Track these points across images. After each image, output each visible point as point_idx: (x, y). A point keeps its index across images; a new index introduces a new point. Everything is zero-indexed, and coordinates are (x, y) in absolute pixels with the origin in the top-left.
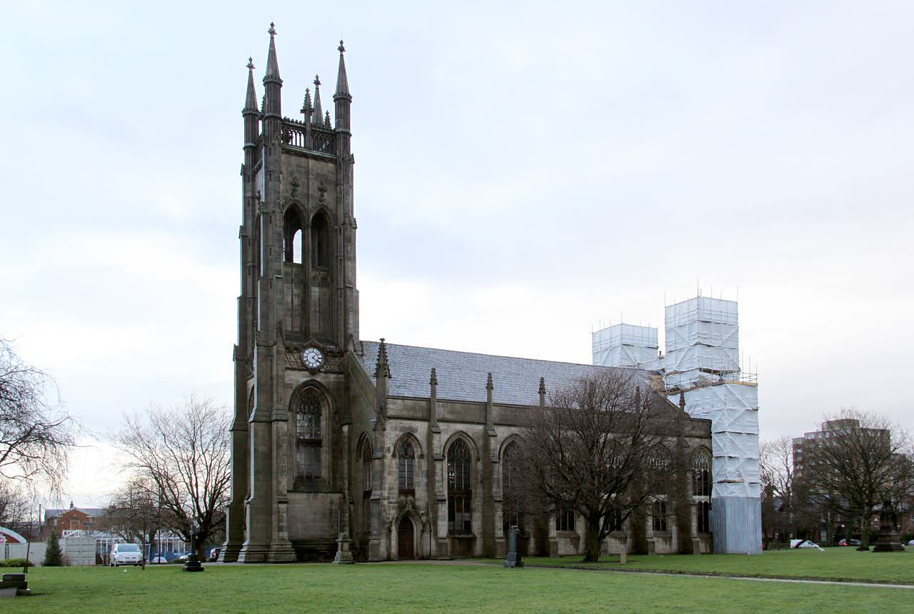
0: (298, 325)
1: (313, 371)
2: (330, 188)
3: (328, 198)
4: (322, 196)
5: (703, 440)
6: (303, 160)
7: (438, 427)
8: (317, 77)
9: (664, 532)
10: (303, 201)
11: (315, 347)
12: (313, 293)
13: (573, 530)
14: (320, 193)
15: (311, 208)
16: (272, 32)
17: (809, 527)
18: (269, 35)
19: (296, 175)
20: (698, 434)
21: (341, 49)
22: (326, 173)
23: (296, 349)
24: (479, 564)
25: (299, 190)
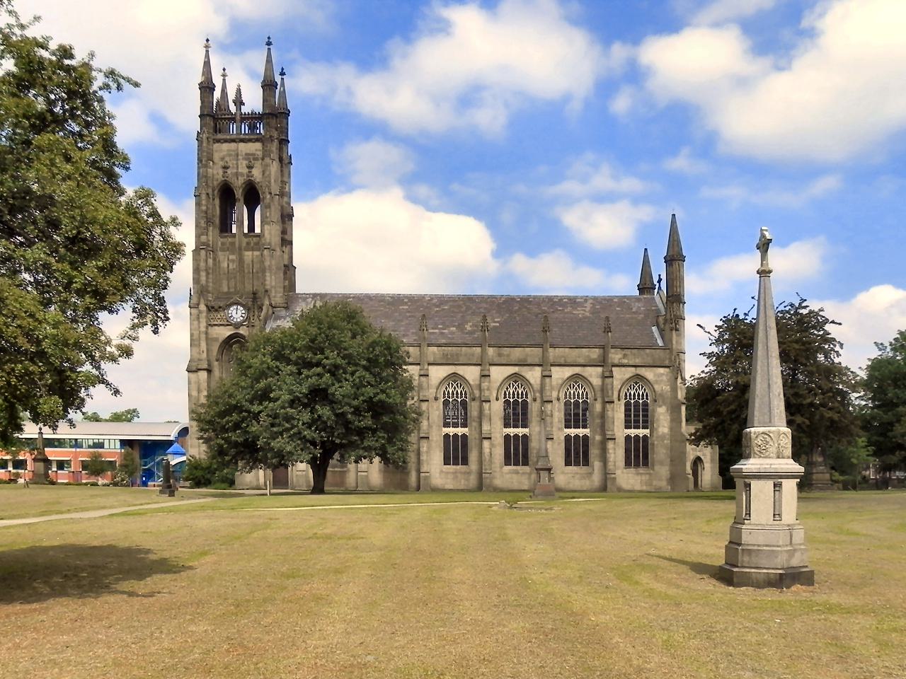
1: (237, 326)
4: (250, 172)
5: (638, 369)
6: (233, 145)
8: (283, 69)
11: (237, 304)
12: (246, 258)
13: (467, 464)
14: (247, 170)
17: (512, 483)
19: (227, 159)
20: (631, 363)
22: (254, 152)
23: (220, 307)
24: (782, 466)
25: (229, 171)
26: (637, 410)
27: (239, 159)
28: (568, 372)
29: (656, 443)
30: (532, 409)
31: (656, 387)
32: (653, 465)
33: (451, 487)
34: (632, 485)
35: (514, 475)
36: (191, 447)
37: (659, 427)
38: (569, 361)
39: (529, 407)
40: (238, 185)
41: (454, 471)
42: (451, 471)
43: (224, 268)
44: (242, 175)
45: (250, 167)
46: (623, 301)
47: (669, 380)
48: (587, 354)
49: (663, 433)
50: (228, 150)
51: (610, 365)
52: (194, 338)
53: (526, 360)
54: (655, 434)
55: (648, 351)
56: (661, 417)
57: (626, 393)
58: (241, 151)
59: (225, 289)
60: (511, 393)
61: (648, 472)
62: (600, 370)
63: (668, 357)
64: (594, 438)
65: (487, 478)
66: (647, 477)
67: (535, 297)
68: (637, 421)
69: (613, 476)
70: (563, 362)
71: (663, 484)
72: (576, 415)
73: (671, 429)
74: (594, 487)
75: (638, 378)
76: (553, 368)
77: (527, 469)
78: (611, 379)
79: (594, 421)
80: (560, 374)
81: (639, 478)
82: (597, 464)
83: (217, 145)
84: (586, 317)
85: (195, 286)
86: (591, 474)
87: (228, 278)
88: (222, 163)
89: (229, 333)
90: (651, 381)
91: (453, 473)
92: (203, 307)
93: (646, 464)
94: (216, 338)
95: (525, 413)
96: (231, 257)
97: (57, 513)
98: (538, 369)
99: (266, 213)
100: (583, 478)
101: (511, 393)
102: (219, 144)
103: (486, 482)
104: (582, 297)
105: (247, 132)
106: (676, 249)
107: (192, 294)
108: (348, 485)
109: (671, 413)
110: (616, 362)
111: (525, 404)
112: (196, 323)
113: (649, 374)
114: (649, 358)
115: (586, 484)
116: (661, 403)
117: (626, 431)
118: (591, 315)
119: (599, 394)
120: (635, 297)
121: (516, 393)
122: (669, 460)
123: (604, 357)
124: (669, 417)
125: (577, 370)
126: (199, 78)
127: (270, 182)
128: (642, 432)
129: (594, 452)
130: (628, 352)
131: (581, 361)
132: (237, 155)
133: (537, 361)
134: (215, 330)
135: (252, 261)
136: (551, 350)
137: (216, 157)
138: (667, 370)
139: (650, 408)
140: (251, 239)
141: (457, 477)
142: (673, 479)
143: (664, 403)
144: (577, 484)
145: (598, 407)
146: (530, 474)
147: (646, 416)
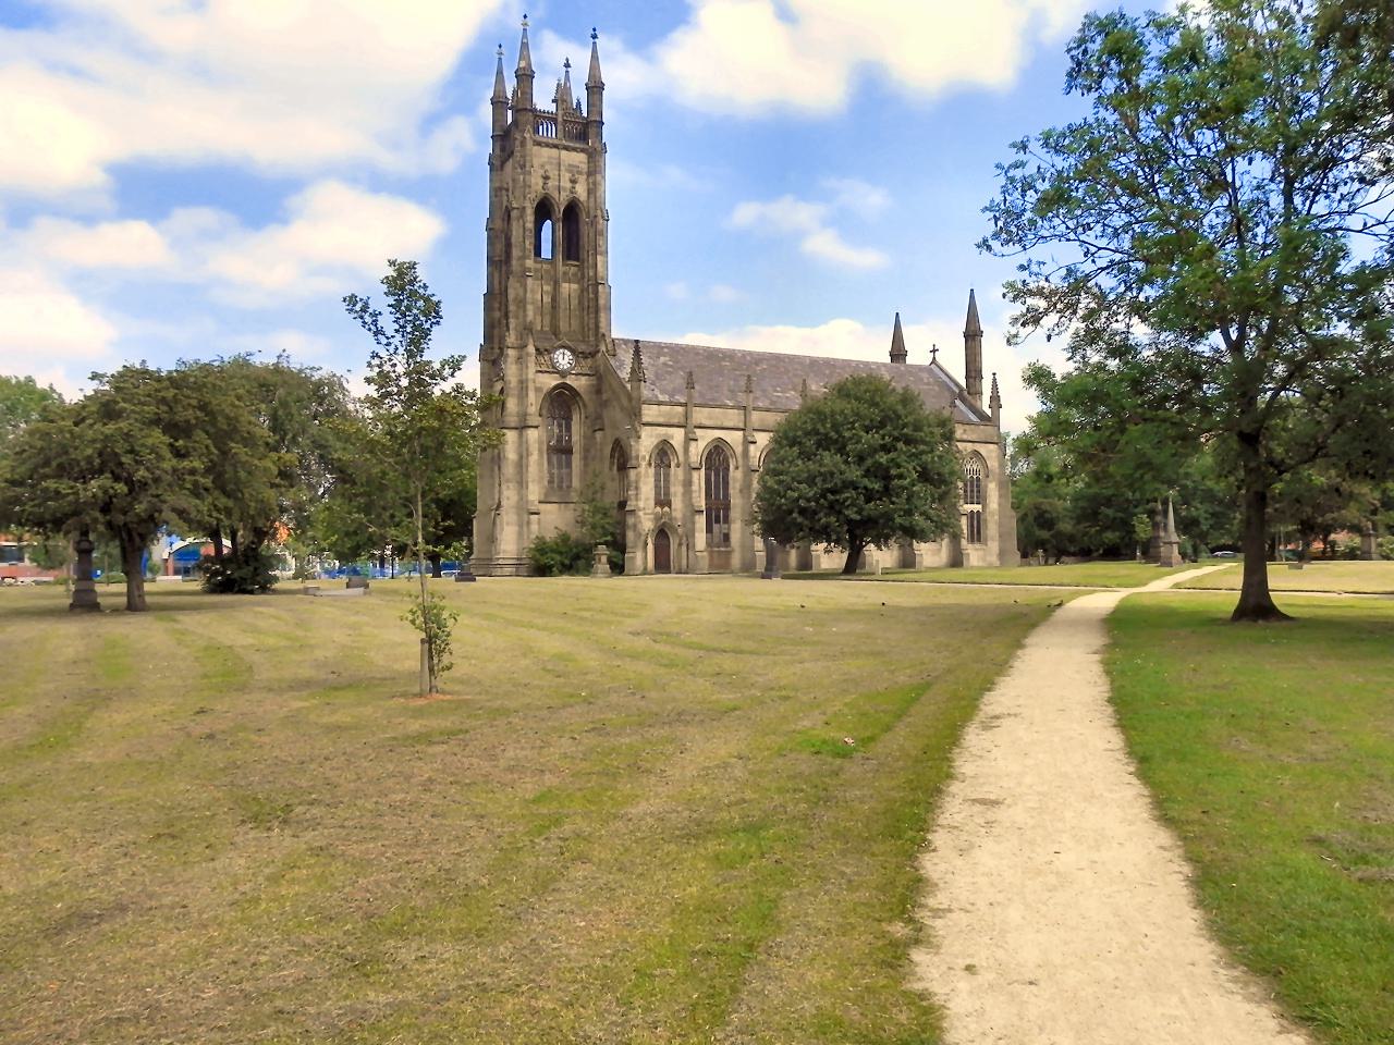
2: (582, 179)
3: (581, 191)
6: (555, 151)
19: (547, 167)
25: (551, 183)
32: (986, 540)
44: (565, 190)
45: (573, 182)
50: (549, 158)
76: (697, 430)
86: (939, 550)
88: (542, 172)
89: (554, 383)
92: (531, 349)
93: (979, 540)
113: (982, 449)
120: (885, 365)
130: (967, 427)
142: (1002, 554)
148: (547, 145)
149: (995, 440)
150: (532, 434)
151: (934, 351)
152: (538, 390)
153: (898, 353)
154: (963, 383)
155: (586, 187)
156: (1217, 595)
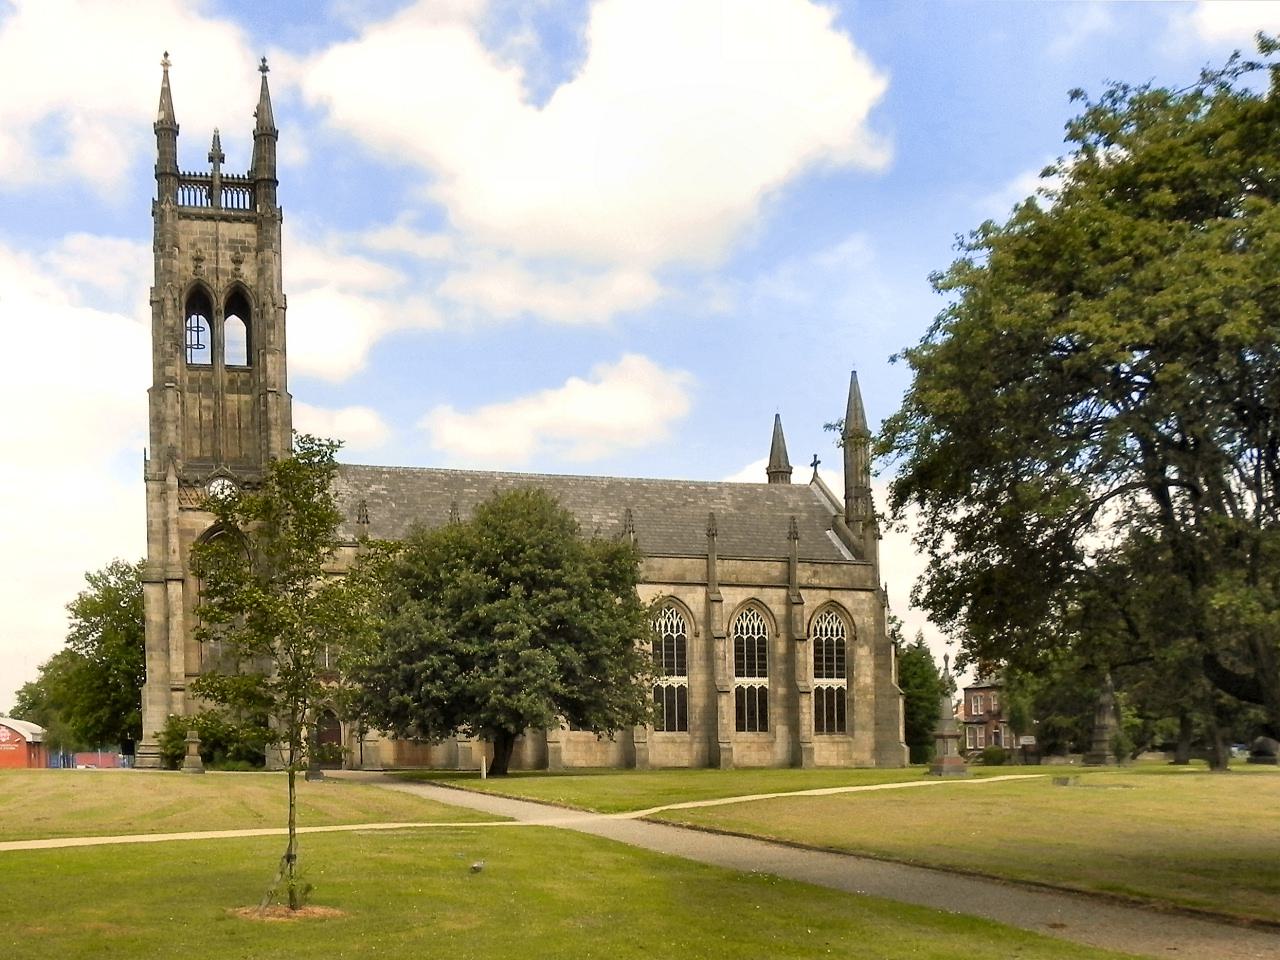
0: (210, 448)
2: (249, 257)
3: (248, 272)
4: (238, 269)
5: (833, 592)
6: (210, 225)
7: (719, 593)
9: (763, 734)
10: (211, 280)
11: (224, 476)
12: (228, 403)
14: (234, 266)
15: (219, 288)
16: (166, 65)
18: (162, 68)
19: (200, 246)
20: (823, 584)
21: (264, 69)
23: (197, 481)
25: (204, 266)
26: (829, 651)
27: (215, 249)
28: (822, 597)
29: (856, 698)
30: (692, 648)
31: (855, 618)
32: (853, 730)
33: (583, 763)
34: (826, 759)
35: (670, 746)
36: (150, 704)
37: (859, 676)
38: (743, 579)
39: (688, 645)
40: (219, 288)
41: (586, 739)
42: (582, 739)
43: (193, 418)
44: (225, 272)
45: (237, 261)
46: (747, 491)
47: (872, 610)
48: (766, 569)
49: (866, 684)
51: (797, 586)
52: (153, 529)
53: (684, 577)
54: (855, 687)
55: (845, 567)
56: (863, 662)
57: (736, 626)
58: (223, 235)
59: (197, 453)
60: (675, 625)
61: (845, 740)
62: (782, 592)
63: (870, 575)
64: (776, 692)
65: (640, 750)
66: (846, 745)
67: (649, 481)
68: (751, 666)
69: (809, 745)
70: (734, 581)
71: (866, 757)
72: (752, 656)
73: (876, 679)
74: (776, 762)
75: (834, 606)
76: (722, 590)
77: (685, 735)
78: (800, 607)
79: (777, 667)
80: (732, 597)
81: (833, 748)
82: (781, 730)
83: (183, 222)
84: (731, 515)
85: (154, 446)
87: (201, 434)
88: (191, 252)
90: (849, 610)
91: (585, 742)
92: (172, 481)
93: (842, 728)
94: (191, 530)
95: (682, 656)
96: (205, 402)
97: (633, 810)
98: (701, 590)
99: (269, 335)
100: (761, 748)
101: (675, 625)
102: (188, 221)
103: (640, 756)
104: (713, 484)
105: (204, 204)
106: (860, 421)
107: (148, 458)
108: (433, 762)
109: (875, 656)
110: (804, 582)
111: (682, 640)
112: (156, 505)
113: (847, 600)
114: (846, 578)
115: (766, 758)
116: (861, 642)
117: (817, 681)
118: (737, 511)
119: (782, 628)
121: (818, 629)
122: (873, 722)
123: (789, 574)
124: (872, 663)
125: (753, 592)
126: (154, 114)
127: (272, 287)
128: (837, 683)
129: (776, 711)
130: (819, 568)
131: (759, 580)
132: (217, 241)
133: (699, 579)
134: (188, 516)
135: (239, 410)
136: (718, 562)
137: (183, 240)
138: (870, 594)
139: (848, 649)
140: (236, 374)
141: (591, 748)
142: (879, 750)
143: (866, 642)
144: (753, 758)
145: (781, 647)
146: (691, 744)
147: (841, 660)
148: (199, 217)
149: (869, 584)
150: (175, 589)
151: (815, 464)
152: (183, 533)
153: (779, 471)
154: (843, 502)
155: (254, 267)
156: (538, 795)
